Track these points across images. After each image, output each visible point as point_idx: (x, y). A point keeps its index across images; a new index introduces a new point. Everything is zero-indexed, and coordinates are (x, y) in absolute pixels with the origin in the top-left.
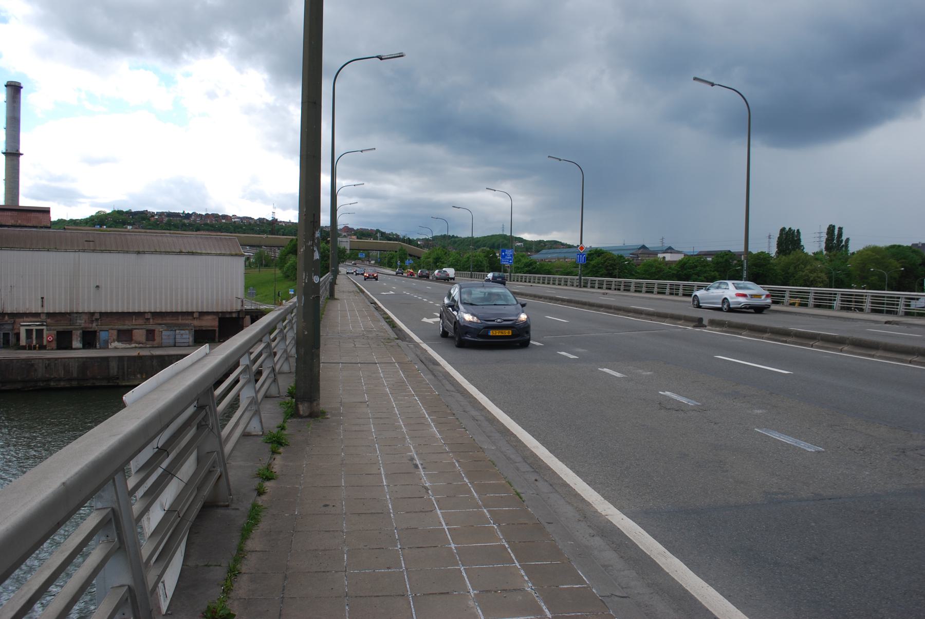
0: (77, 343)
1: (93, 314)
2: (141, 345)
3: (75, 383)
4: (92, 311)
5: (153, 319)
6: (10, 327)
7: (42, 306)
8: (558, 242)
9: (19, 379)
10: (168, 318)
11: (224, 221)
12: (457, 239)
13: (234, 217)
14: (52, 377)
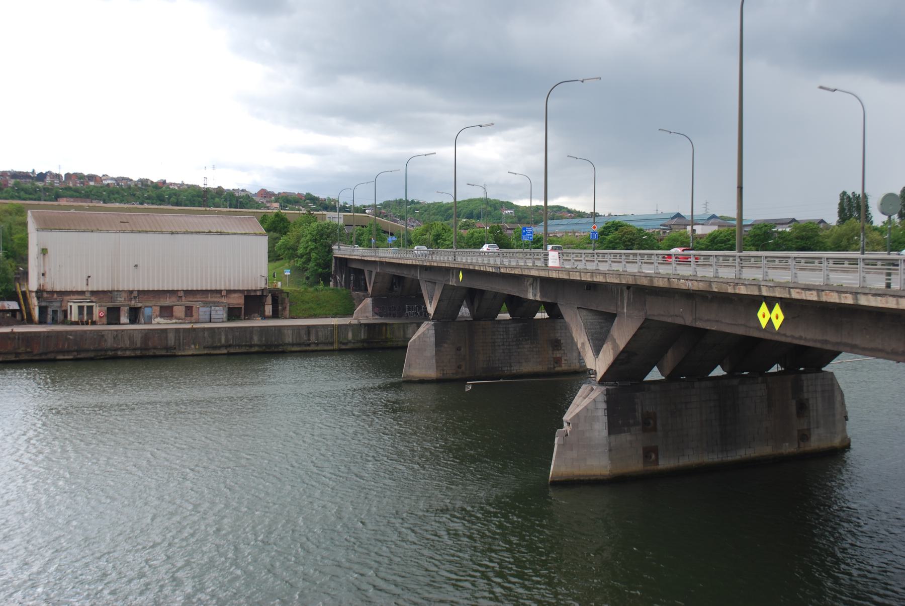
0: (124, 319)
1: (131, 292)
2: (180, 321)
3: (138, 353)
4: (131, 289)
5: (185, 297)
6: (58, 304)
7: (87, 284)
8: (564, 208)
9: (92, 349)
10: (198, 296)
11: (92, 183)
12: (418, 206)
13: (104, 178)
14: (120, 347)
